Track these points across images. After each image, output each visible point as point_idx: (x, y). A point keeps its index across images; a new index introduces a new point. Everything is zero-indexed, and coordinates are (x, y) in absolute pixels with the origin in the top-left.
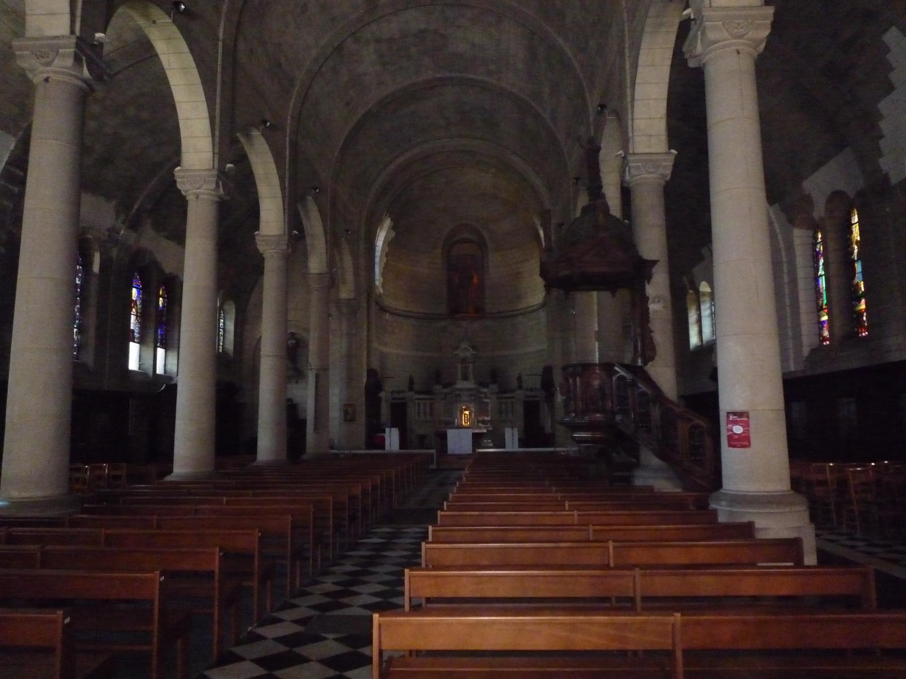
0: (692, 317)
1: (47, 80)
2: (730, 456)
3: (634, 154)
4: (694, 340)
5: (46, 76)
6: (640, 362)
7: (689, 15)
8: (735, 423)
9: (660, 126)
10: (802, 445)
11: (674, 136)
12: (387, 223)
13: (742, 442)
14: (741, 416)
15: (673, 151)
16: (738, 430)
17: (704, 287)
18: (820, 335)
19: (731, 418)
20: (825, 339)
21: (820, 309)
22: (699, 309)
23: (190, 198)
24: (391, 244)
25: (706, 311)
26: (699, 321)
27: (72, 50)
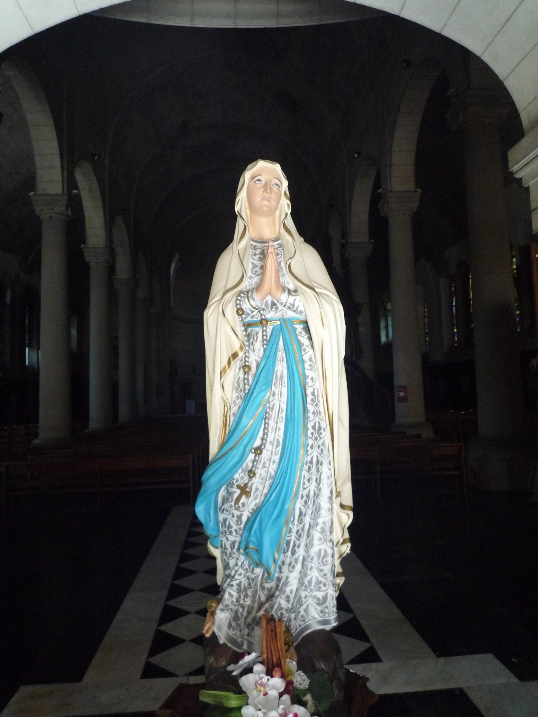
0: (382, 325)
1: (51, 217)
2: (400, 407)
3: (351, 243)
4: (383, 339)
5: (50, 215)
6: (354, 359)
7: (381, 192)
8: (401, 391)
9: (365, 227)
10: (431, 401)
11: (372, 234)
12: (177, 257)
13: (404, 400)
14: (403, 388)
15: (372, 241)
16: (402, 394)
17: (389, 306)
18: (453, 339)
19: (399, 389)
20: (455, 342)
21: (452, 325)
22: (386, 320)
23: (93, 265)
24: (177, 271)
25: (390, 319)
26: (387, 327)
27: (65, 202)
